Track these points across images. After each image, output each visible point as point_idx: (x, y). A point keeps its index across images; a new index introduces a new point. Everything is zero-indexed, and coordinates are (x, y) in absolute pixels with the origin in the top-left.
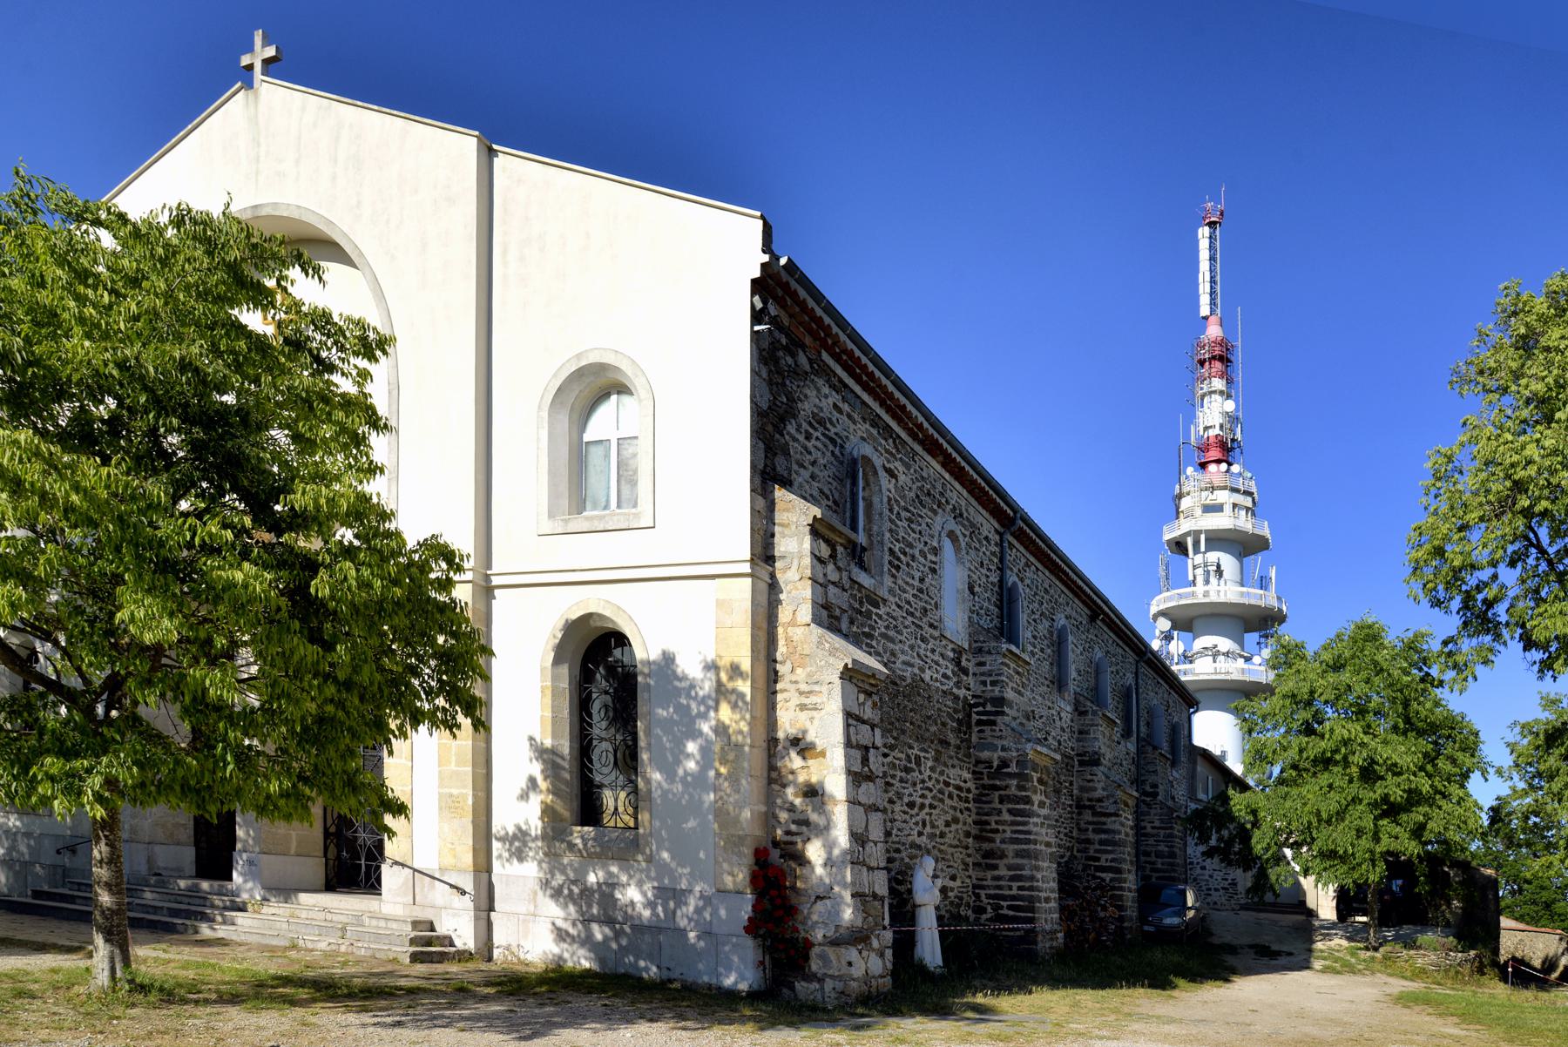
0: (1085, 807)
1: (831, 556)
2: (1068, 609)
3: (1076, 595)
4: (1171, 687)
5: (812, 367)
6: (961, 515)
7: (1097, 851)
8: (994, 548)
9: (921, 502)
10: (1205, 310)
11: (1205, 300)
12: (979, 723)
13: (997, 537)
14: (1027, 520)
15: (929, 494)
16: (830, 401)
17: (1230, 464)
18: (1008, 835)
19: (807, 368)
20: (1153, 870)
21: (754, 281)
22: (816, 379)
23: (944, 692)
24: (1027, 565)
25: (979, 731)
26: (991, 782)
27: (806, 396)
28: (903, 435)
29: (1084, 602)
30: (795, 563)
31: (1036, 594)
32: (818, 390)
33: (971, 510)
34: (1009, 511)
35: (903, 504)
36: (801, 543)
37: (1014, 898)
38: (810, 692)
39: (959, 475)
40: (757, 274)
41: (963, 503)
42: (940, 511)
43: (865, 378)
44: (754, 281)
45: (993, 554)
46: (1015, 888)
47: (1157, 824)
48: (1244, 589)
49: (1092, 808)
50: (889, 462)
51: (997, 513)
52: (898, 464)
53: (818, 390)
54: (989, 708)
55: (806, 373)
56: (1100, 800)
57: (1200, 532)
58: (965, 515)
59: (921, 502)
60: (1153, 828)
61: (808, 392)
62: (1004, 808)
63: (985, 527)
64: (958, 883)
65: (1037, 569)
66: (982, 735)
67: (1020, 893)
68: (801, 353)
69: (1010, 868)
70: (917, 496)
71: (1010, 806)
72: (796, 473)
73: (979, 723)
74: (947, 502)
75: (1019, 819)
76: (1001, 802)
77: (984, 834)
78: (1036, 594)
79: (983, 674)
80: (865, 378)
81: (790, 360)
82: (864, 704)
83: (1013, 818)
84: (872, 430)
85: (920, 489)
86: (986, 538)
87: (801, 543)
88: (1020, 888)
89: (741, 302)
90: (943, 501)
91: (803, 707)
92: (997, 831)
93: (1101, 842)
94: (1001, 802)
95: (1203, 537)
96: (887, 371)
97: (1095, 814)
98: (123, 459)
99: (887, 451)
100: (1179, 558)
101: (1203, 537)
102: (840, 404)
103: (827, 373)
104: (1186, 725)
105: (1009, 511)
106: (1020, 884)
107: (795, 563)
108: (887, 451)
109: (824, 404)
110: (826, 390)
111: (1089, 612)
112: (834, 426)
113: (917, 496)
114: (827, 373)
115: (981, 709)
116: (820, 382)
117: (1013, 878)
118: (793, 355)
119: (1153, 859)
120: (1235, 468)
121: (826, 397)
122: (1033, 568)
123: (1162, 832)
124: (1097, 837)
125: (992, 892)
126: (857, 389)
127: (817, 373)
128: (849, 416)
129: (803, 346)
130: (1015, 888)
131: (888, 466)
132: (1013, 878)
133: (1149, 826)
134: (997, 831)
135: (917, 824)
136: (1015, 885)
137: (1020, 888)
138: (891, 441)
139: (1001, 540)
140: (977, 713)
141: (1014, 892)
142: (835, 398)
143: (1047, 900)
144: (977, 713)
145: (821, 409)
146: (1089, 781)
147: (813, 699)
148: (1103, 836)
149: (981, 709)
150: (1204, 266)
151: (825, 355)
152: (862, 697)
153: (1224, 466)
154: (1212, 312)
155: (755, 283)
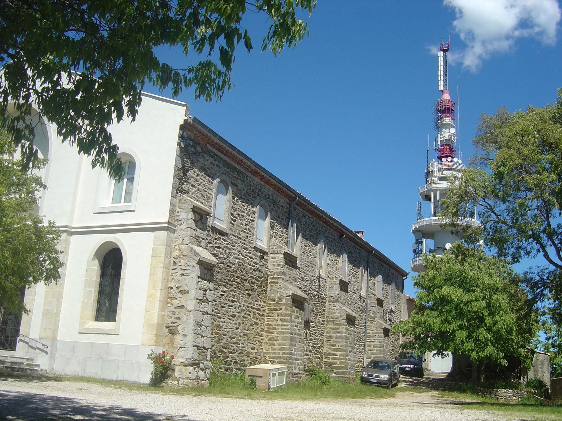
0: (330, 321)
1: (200, 219)
2: (327, 234)
3: (331, 227)
4: (390, 267)
5: (202, 150)
6: (269, 198)
7: (334, 342)
8: (285, 210)
9: (249, 195)
10: (441, 88)
11: (441, 83)
12: (272, 282)
13: (288, 205)
14: (301, 197)
15: (253, 191)
16: (209, 161)
17: (453, 158)
18: (280, 330)
19: (201, 151)
20: (372, 354)
21: (181, 125)
22: (204, 154)
23: (254, 270)
24: (304, 216)
25: (271, 286)
26: (274, 308)
27: (199, 161)
28: (242, 170)
29: (335, 230)
30: (185, 222)
31: (308, 228)
32: (204, 158)
33: (274, 196)
34: (293, 195)
35: (240, 196)
36: (188, 215)
37: (280, 358)
38: (185, 269)
39: (268, 182)
40: (182, 123)
41: (270, 193)
42: (258, 197)
43: (225, 152)
44: (181, 125)
45: (286, 212)
46: (281, 354)
47: (375, 331)
48: (437, 218)
49: (333, 321)
50: (234, 180)
51: (287, 196)
52: (239, 181)
53: (204, 158)
54: (276, 276)
55: (200, 153)
56: (337, 318)
57: (437, 190)
58: (271, 197)
59: (249, 195)
60: (373, 333)
61: (199, 159)
62: (279, 318)
63: (281, 201)
64: (255, 351)
65: (309, 217)
66: (272, 287)
67: (284, 355)
68: (198, 146)
69: (279, 345)
70: (247, 192)
71: (282, 318)
72: (191, 189)
73: (272, 282)
74: (262, 193)
75: (285, 323)
76: (278, 316)
77: (270, 330)
78: (308, 228)
79: (274, 262)
80: (225, 152)
81: (193, 150)
82: (206, 274)
83: (282, 323)
84: (227, 169)
85: (250, 189)
86: (282, 206)
87: (188, 215)
88: (283, 353)
89: (176, 132)
90: (260, 193)
91: (182, 275)
92: (275, 329)
93: (337, 338)
94: (278, 316)
95: (438, 193)
96: (234, 148)
97: (334, 324)
98: (281, 374)
99: (234, 177)
100: (426, 202)
101: (438, 193)
102: (214, 162)
103: (208, 152)
104: (401, 286)
105: (293, 195)
106: (284, 352)
107: (185, 222)
108: (234, 177)
109: (206, 163)
110: (208, 158)
111: (339, 234)
112: (210, 170)
113: (247, 192)
114: (208, 152)
115: (272, 276)
116: (205, 155)
117: (280, 349)
118: (194, 147)
119: (372, 348)
120: (455, 160)
121: (208, 160)
122: (307, 217)
123: (377, 335)
124: (335, 335)
125: (271, 355)
126: (222, 156)
127: (205, 152)
128: (217, 166)
129: (199, 144)
130: (281, 354)
131: (234, 182)
132: (280, 349)
133: (371, 332)
134: (275, 329)
135: (235, 324)
136: (281, 352)
137: (283, 353)
138: (236, 173)
139: (290, 207)
140: (271, 279)
141: (281, 355)
142: (212, 160)
143: (297, 359)
144: (271, 279)
145: (205, 165)
146: (332, 309)
147: (186, 272)
148: (338, 335)
149: (272, 276)
150: (441, 68)
151: (208, 146)
152: (206, 271)
153: (449, 159)
154: (445, 88)
155: (181, 126)
